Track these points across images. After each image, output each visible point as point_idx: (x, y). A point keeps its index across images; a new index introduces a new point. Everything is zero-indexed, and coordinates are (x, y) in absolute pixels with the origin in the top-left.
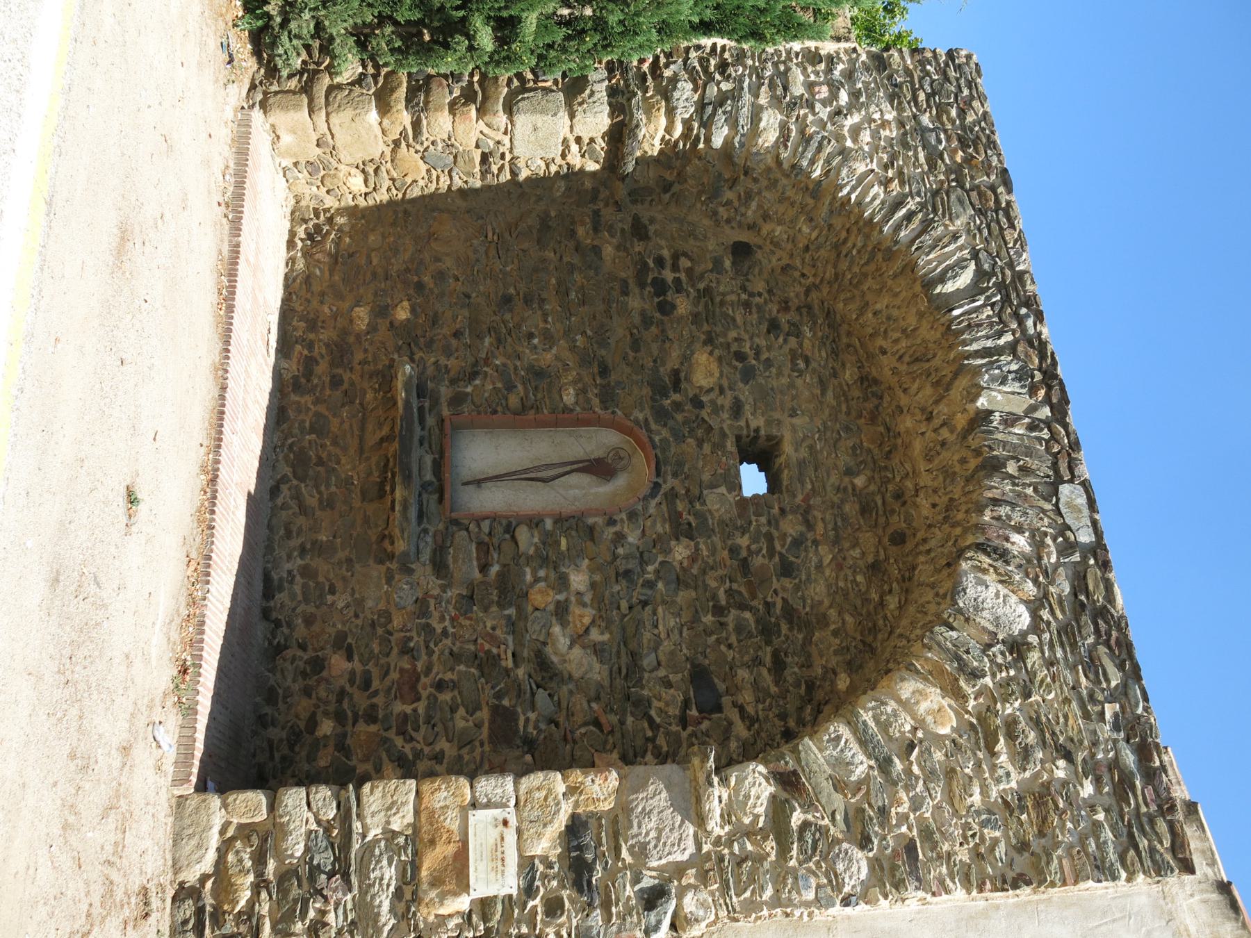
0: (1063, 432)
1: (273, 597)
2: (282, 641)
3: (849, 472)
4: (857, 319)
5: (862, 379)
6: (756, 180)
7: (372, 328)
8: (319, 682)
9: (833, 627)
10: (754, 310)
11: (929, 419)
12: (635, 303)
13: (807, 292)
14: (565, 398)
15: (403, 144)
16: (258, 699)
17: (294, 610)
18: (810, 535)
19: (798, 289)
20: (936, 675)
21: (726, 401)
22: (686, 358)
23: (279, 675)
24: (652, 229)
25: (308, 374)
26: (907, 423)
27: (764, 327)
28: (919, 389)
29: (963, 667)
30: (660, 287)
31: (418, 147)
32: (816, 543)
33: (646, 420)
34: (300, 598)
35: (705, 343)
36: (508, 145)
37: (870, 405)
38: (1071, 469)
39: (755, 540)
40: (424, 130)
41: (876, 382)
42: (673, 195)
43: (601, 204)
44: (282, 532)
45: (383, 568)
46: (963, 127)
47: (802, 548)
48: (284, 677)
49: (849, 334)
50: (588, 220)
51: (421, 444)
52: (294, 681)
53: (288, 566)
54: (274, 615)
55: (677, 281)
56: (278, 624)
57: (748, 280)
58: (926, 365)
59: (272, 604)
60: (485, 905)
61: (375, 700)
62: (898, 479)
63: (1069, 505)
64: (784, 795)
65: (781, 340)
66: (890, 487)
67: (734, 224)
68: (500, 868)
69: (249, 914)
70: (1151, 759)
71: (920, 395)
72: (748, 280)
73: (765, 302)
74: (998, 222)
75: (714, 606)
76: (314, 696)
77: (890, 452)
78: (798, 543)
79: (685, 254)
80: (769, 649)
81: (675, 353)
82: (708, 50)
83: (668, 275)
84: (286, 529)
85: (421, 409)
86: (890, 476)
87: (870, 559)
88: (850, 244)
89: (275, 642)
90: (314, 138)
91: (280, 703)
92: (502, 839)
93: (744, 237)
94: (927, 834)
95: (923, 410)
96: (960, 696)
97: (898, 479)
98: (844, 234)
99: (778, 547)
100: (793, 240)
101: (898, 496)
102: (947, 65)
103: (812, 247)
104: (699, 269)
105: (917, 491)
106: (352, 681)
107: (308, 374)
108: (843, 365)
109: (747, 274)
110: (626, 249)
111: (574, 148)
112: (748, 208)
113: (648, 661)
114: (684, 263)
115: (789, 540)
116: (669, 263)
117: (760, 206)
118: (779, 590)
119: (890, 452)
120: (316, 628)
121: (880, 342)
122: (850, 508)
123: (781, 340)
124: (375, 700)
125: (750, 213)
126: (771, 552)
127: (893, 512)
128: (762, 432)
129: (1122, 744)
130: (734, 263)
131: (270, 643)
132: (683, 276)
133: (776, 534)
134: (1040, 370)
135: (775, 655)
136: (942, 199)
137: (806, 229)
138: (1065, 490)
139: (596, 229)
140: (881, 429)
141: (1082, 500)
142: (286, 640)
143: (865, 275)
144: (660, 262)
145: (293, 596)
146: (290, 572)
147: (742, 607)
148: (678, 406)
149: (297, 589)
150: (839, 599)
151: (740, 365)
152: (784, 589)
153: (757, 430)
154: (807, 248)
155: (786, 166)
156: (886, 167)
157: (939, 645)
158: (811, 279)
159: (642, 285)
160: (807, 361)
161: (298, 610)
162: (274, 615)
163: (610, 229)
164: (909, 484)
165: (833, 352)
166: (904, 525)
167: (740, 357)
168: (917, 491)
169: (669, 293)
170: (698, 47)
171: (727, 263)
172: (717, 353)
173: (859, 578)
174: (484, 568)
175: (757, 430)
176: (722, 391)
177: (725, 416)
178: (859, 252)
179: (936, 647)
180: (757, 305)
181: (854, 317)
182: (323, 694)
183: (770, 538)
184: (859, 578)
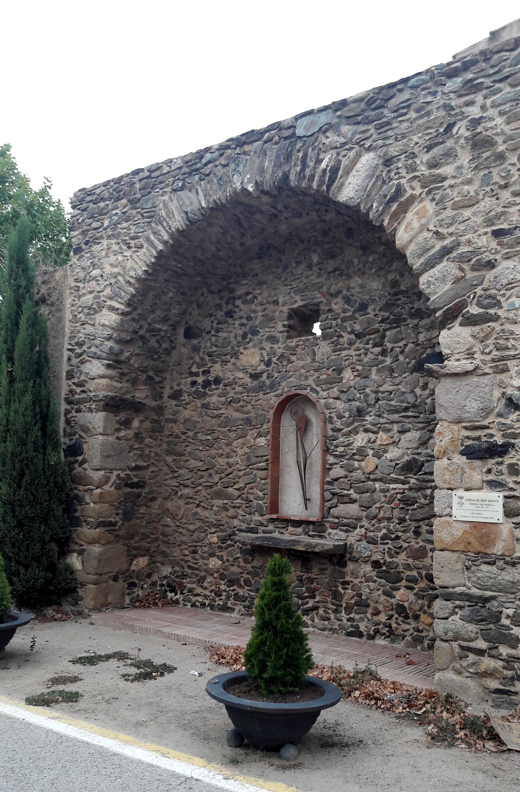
0: (267, 134)
1: (361, 632)
2: (387, 629)
3: (310, 267)
4: (225, 261)
5: (259, 258)
6: (141, 327)
7: (220, 558)
8: (411, 609)
9: (398, 277)
10: (220, 326)
11: (276, 216)
12: (214, 399)
13: (212, 293)
14: (262, 444)
15: (118, 533)
16: (419, 648)
17: (369, 620)
18: (344, 292)
19: (209, 298)
20: (398, 216)
21: (267, 346)
22: (244, 370)
23: (406, 634)
24: (176, 388)
25: (243, 599)
26: (283, 228)
27: (230, 320)
28: (259, 222)
29: (393, 199)
30: (207, 384)
31: (119, 524)
32: (349, 289)
33: (276, 396)
34: (362, 615)
35: (237, 358)
36: (119, 472)
37: (274, 253)
38: (289, 128)
39: (344, 329)
40: (108, 520)
41: (261, 248)
42: (156, 375)
43: (162, 418)
44: (326, 623)
45: (349, 563)
46: (110, 199)
47: (351, 298)
48: (407, 630)
49: (235, 266)
50: (170, 425)
51: (282, 533)
52: (410, 624)
53: (345, 621)
54: (372, 632)
55: (204, 372)
56: (377, 631)
57: (205, 329)
58: (243, 220)
59: (365, 633)
60: (508, 513)
61: (423, 575)
62: (315, 234)
63: (307, 128)
64: (460, 319)
65: (237, 310)
66: (320, 239)
67: (173, 338)
68: (487, 503)
69: (509, 662)
70: (455, 68)
71: (263, 221)
72: (205, 329)
73: (216, 319)
74: (157, 177)
75: (382, 356)
76: (418, 613)
77: (300, 239)
78: (348, 300)
79: (190, 368)
80: (409, 321)
81: (240, 375)
82: (70, 353)
83: (200, 379)
84: (324, 620)
85: (264, 532)
86: (313, 239)
87: (361, 252)
88: (175, 268)
89: (388, 634)
90: (111, 582)
91: (422, 634)
92: (469, 500)
93: (181, 331)
94: (490, 222)
95: (270, 220)
96: (412, 199)
97: (315, 234)
98: (170, 272)
99: (350, 314)
100: (179, 303)
101: (325, 233)
102: (79, 209)
103: (182, 291)
104: (198, 360)
105: (322, 221)
106: (411, 589)
107: (243, 599)
108: (251, 269)
109: (201, 330)
110: (187, 404)
111: (122, 434)
112: (160, 330)
113: (410, 399)
114: (194, 369)
115: (346, 307)
116: (194, 379)
117: (159, 322)
118: (374, 313)
119: (300, 239)
120: (381, 608)
121: (237, 245)
122: (331, 265)
123: (237, 310)
124: (423, 575)
125: (164, 328)
126: (352, 318)
127: (334, 237)
128: (286, 323)
129: (446, 89)
130: (195, 338)
131: (388, 637)
132: (201, 370)
133: (343, 315)
134: (235, 149)
135: (412, 316)
136: (145, 212)
137: (170, 295)
138: (300, 132)
139: (175, 421)
140: (287, 245)
141: (305, 121)
142: (386, 627)
143: (194, 258)
144: (194, 383)
145: (362, 620)
146: (348, 620)
147: (383, 337)
148: (269, 376)
149: (357, 617)
150: (382, 273)
151: (249, 336)
152: (374, 310)
153: (284, 326)
154: (183, 293)
155: (128, 309)
156: (129, 248)
157: (381, 215)
158: (205, 290)
159: (205, 394)
160: (248, 293)
161: (370, 618)
162: (372, 632)
163: (175, 413)
164: (318, 226)
165: (244, 276)
166: (341, 229)
167: (244, 336)
168: (322, 221)
169: (210, 379)
170: (69, 359)
171: (195, 342)
172: (242, 350)
173: (371, 259)
174: (353, 501)
175: (284, 326)
176: (262, 349)
177: (276, 346)
178: (180, 263)
179: (381, 218)
180: (218, 324)
181: (224, 262)
182: (417, 607)
183: (344, 320)
184: (371, 259)
